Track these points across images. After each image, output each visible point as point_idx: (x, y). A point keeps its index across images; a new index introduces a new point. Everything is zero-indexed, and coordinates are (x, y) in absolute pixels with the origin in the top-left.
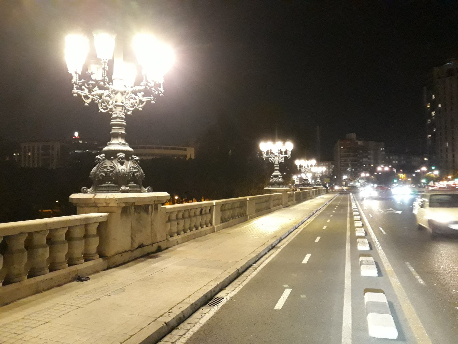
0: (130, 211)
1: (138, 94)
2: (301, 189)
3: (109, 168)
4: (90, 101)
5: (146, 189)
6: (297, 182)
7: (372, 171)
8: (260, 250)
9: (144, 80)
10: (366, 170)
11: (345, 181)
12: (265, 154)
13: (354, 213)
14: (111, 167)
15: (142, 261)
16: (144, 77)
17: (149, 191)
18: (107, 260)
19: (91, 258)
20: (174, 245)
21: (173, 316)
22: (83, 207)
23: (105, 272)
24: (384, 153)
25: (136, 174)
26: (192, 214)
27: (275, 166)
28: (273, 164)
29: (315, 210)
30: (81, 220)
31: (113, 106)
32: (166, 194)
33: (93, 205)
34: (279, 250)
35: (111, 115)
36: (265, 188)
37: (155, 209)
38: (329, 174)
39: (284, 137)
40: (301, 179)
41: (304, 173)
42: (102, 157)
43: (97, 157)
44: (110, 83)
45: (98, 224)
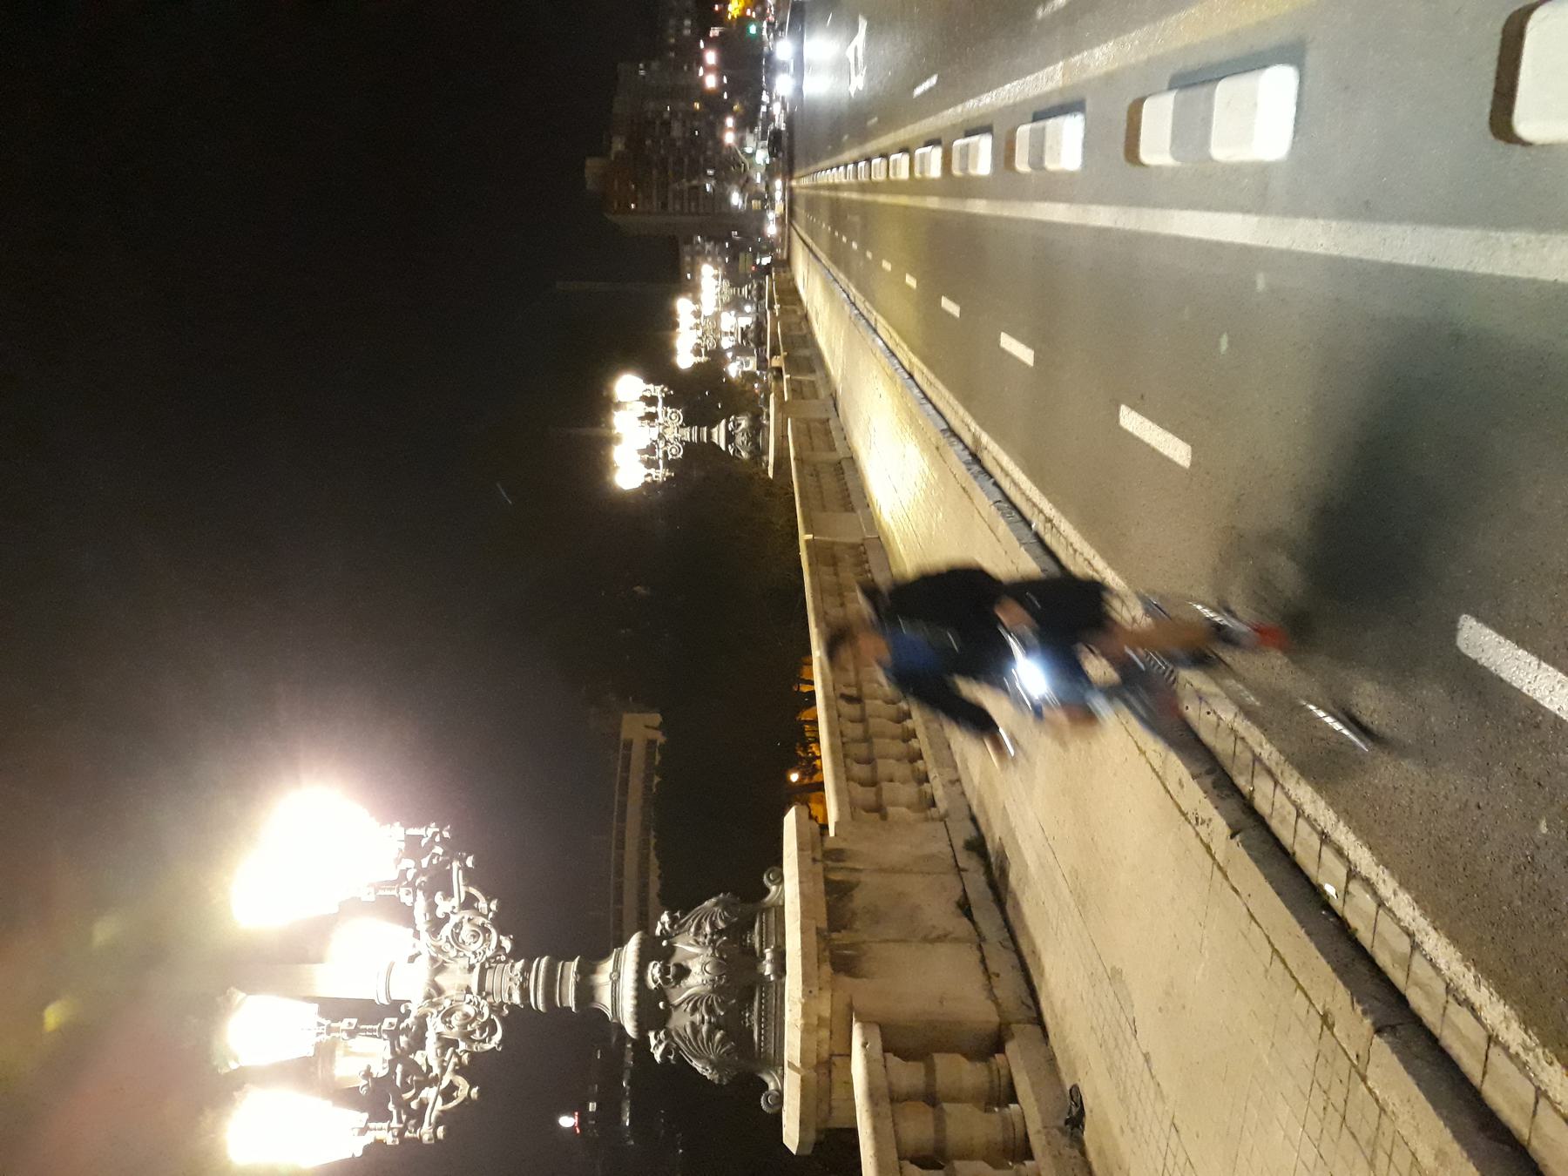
0: (846, 947)
1: (440, 914)
2: (775, 352)
3: (698, 1017)
4: (461, 1081)
5: (773, 888)
6: (747, 364)
7: (716, 106)
8: (984, 502)
9: (394, 892)
10: (715, 128)
11: (749, 201)
12: (652, 471)
13: (863, 177)
14: (695, 1009)
15: (1017, 905)
16: (381, 893)
17: (780, 879)
18: (1014, 1027)
19: (1004, 1081)
20: (963, 793)
21: (1207, 809)
22: (831, 1109)
23: (1051, 1036)
24: (655, 65)
25: (721, 925)
26: (855, 730)
27: (695, 438)
28: (688, 447)
29: (847, 307)
30: (875, 1116)
31: (483, 1002)
32: (790, 820)
33: (826, 1072)
34: (985, 438)
35: (512, 1007)
36: (771, 474)
37: (838, 861)
38: (723, 253)
39: (602, 405)
40: (739, 350)
41: (718, 342)
42: (660, 1042)
43: (658, 1059)
44: (403, 1010)
45: (890, 1056)
